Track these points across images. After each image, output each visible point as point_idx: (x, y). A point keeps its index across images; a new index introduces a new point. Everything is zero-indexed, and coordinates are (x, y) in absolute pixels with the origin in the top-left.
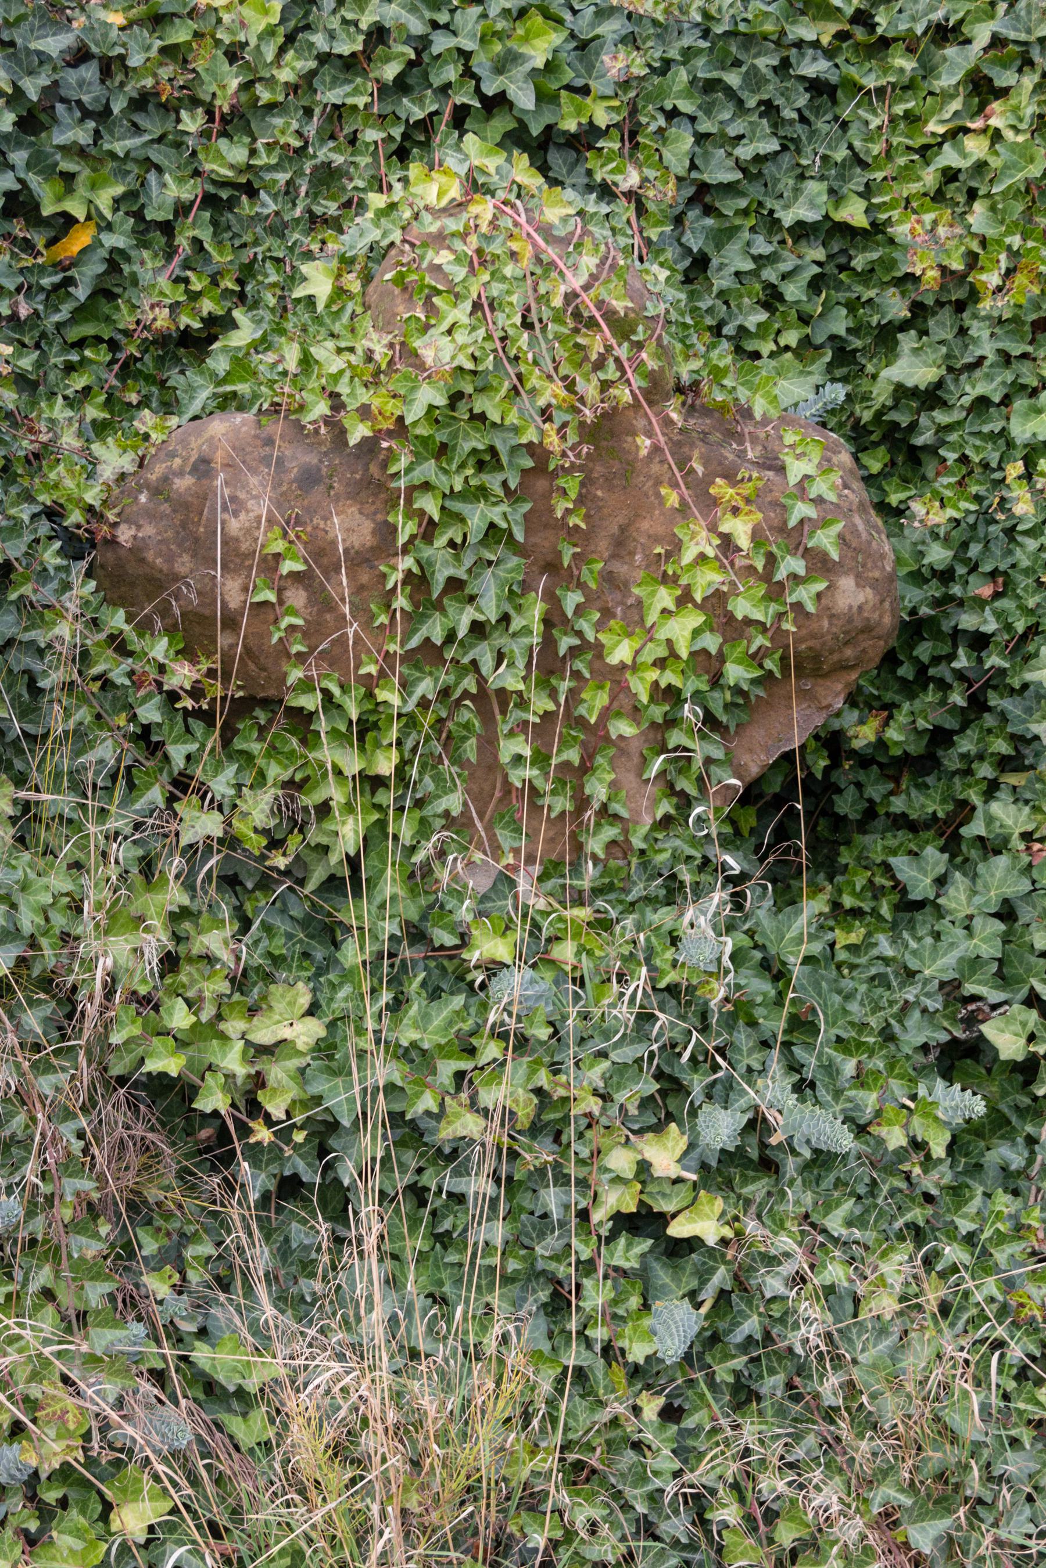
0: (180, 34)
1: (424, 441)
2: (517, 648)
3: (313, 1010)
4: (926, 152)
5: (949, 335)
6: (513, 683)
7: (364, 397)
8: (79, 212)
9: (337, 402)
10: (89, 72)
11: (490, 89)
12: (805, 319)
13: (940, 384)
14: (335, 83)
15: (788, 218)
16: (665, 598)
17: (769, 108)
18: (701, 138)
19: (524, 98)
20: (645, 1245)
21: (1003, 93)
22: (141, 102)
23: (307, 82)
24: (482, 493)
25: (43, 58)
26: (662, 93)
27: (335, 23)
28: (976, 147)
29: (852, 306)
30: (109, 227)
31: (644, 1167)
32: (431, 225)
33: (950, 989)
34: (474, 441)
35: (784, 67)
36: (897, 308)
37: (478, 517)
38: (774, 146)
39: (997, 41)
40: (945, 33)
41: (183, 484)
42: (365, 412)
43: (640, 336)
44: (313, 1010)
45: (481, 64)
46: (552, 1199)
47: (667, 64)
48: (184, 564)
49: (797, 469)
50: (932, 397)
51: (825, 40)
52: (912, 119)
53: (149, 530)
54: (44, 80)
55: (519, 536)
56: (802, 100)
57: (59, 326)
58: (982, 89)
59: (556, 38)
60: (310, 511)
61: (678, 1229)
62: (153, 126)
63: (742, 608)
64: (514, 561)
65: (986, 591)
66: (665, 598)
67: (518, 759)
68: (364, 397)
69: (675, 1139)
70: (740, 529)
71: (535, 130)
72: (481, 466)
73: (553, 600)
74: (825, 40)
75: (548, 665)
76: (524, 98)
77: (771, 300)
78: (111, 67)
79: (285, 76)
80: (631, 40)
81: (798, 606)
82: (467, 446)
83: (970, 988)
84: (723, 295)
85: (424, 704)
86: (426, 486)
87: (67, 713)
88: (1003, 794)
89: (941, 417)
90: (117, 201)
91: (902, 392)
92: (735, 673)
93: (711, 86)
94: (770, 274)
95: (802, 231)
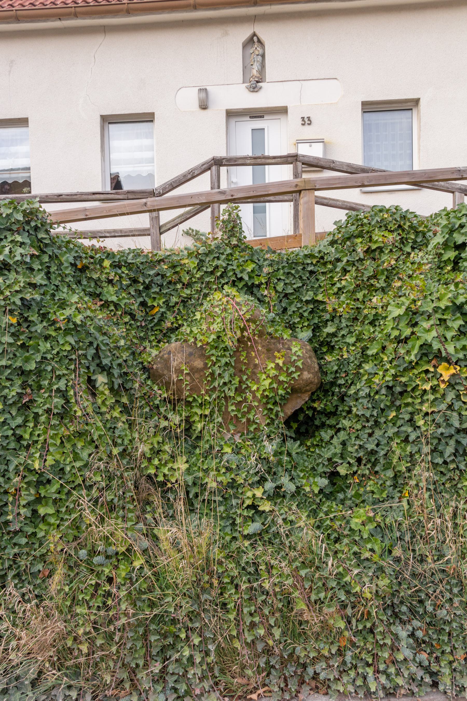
0: (178, 269)
1: (213, 346)
2: (233, 388)
3: (187, 462)
4: (333, 285)
5: (338, 322)
6: (232, 395)
7: (202, 338)
8: (156, 305)
9: (196, 339)
10: (159, 277)
11: (239, 276)
12: (308, 320)
13: (336, 332)
14: (208, 277)
15: (304, 299)
16: (264, 376)
17: (301, 278)
18: (285, 284)
19: (246, 278)
20: (253, 512)
21: (349, 271)
22: (170, 283)
23: (202, 278)
24: (225, 356)
25: (149, 275)
26: (276, 275)
27: (208, 265)
28: (344, 283)
29: (319, 317)
30: (162, 307)
31: (254, 495)
32: (216, 303)
33: (330, 460)
34: (222, 346)
35: (304, 269)
36: (328, 317)
37: (224, 360)
38: (301, 285)
39: (348, 261)
40: (338, 260)
41: (166, 356)
42: (201, 341)
43: (258, 323)
44: (187, 462)
45: (238, 271)
46: (234, 502)
47: (278, 269)
48: (165, 372)
49: (294, 350)
50: (334, 335)
51: (314, 263)
52: (332, 277)
53: (159, 366)
54: (149, 279)
55: (233, 364)
56: (308, 275)
57: (152, 327)
58: (345, 271)
59: (253, 265)
60: (191, 361)
61: (261, 509)
62: (172, 287)
63: (282, 378)
64: (232, 369)
65: (344, 375)
66: (264, 376)
67: (233, 410)
68: (202, 338)
69: (261, 490)
70: (280, 362)
71: (249, 284)
72: (225, 350)
73: (241, 378)
74: (314, 263)
75: (239, 390)
76: (246, 278)
77: (301, 316)
78: (163, 276)
79: (198, 276)
80: (271, 265)
81: (294, 378)
82: (221, 346)
83: (335, 460)
84: (290, 315)
85: (215, 400)
86: (213, 355)
87: (140, 402)
88: (347, 419)
89: (336, 339)
90: (164, 303)
91: (328, 335)
92: (281, 392)
93: (288, 273)
94: (301, 311)
95: (307, 302)
